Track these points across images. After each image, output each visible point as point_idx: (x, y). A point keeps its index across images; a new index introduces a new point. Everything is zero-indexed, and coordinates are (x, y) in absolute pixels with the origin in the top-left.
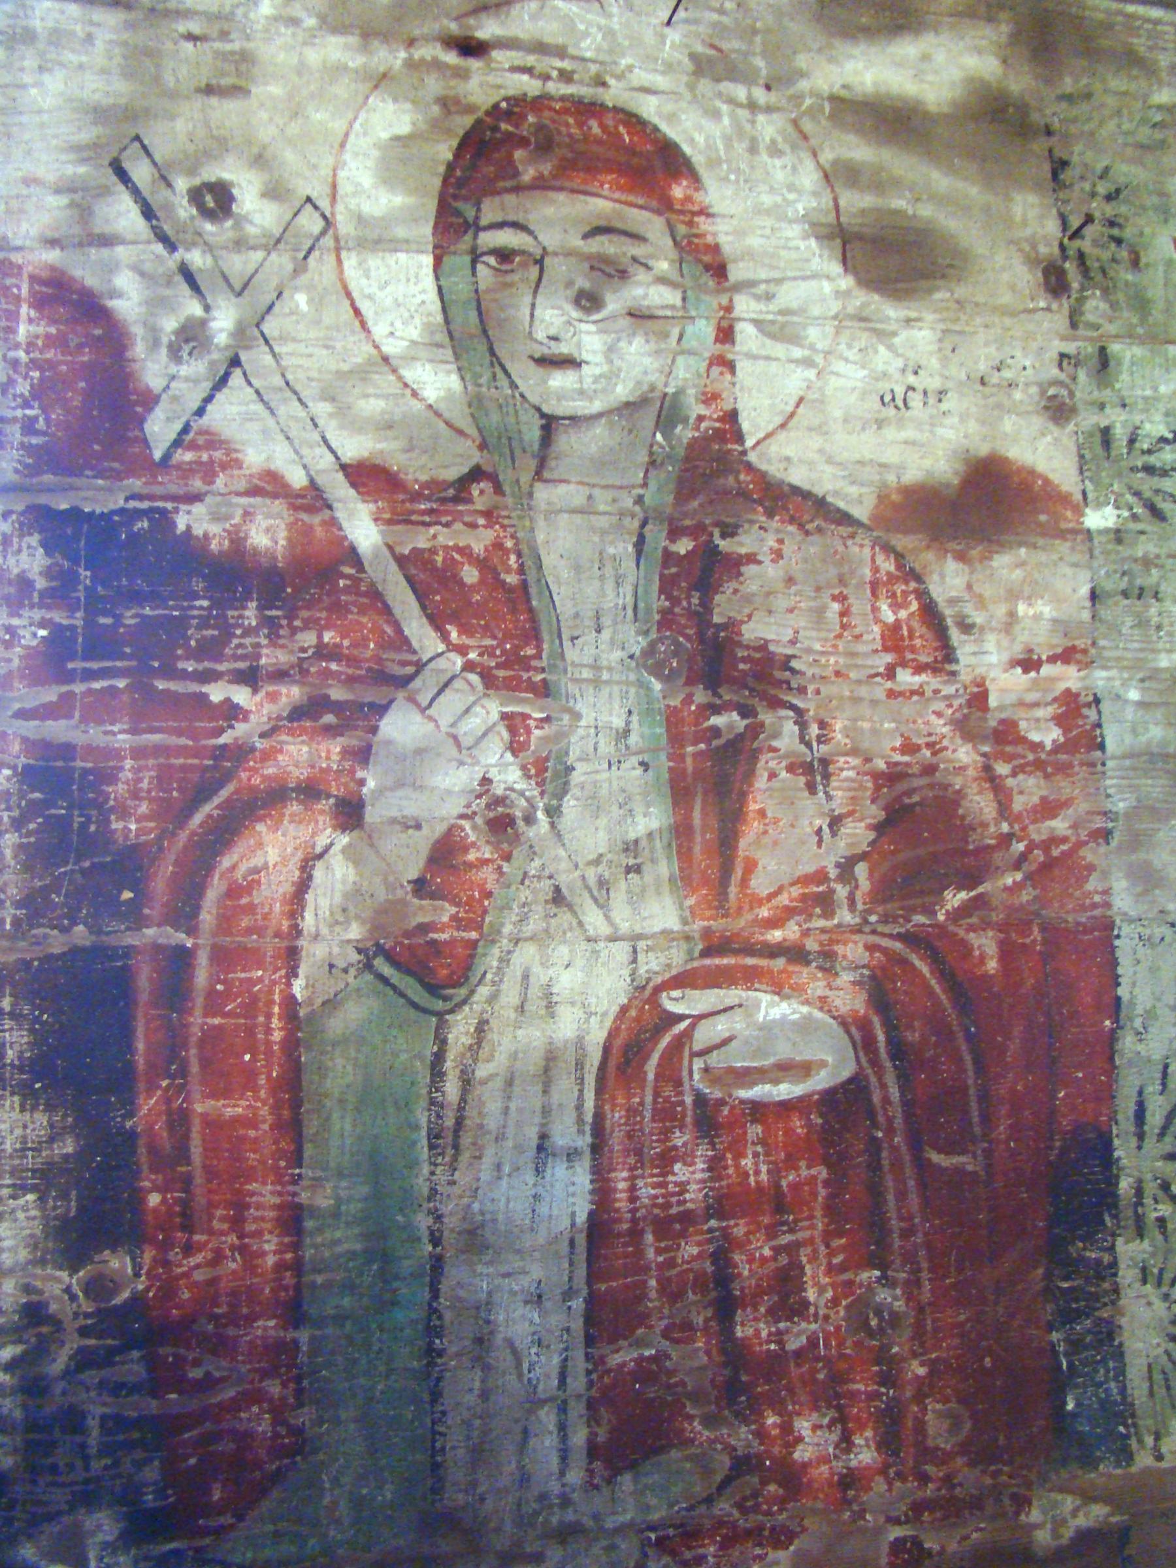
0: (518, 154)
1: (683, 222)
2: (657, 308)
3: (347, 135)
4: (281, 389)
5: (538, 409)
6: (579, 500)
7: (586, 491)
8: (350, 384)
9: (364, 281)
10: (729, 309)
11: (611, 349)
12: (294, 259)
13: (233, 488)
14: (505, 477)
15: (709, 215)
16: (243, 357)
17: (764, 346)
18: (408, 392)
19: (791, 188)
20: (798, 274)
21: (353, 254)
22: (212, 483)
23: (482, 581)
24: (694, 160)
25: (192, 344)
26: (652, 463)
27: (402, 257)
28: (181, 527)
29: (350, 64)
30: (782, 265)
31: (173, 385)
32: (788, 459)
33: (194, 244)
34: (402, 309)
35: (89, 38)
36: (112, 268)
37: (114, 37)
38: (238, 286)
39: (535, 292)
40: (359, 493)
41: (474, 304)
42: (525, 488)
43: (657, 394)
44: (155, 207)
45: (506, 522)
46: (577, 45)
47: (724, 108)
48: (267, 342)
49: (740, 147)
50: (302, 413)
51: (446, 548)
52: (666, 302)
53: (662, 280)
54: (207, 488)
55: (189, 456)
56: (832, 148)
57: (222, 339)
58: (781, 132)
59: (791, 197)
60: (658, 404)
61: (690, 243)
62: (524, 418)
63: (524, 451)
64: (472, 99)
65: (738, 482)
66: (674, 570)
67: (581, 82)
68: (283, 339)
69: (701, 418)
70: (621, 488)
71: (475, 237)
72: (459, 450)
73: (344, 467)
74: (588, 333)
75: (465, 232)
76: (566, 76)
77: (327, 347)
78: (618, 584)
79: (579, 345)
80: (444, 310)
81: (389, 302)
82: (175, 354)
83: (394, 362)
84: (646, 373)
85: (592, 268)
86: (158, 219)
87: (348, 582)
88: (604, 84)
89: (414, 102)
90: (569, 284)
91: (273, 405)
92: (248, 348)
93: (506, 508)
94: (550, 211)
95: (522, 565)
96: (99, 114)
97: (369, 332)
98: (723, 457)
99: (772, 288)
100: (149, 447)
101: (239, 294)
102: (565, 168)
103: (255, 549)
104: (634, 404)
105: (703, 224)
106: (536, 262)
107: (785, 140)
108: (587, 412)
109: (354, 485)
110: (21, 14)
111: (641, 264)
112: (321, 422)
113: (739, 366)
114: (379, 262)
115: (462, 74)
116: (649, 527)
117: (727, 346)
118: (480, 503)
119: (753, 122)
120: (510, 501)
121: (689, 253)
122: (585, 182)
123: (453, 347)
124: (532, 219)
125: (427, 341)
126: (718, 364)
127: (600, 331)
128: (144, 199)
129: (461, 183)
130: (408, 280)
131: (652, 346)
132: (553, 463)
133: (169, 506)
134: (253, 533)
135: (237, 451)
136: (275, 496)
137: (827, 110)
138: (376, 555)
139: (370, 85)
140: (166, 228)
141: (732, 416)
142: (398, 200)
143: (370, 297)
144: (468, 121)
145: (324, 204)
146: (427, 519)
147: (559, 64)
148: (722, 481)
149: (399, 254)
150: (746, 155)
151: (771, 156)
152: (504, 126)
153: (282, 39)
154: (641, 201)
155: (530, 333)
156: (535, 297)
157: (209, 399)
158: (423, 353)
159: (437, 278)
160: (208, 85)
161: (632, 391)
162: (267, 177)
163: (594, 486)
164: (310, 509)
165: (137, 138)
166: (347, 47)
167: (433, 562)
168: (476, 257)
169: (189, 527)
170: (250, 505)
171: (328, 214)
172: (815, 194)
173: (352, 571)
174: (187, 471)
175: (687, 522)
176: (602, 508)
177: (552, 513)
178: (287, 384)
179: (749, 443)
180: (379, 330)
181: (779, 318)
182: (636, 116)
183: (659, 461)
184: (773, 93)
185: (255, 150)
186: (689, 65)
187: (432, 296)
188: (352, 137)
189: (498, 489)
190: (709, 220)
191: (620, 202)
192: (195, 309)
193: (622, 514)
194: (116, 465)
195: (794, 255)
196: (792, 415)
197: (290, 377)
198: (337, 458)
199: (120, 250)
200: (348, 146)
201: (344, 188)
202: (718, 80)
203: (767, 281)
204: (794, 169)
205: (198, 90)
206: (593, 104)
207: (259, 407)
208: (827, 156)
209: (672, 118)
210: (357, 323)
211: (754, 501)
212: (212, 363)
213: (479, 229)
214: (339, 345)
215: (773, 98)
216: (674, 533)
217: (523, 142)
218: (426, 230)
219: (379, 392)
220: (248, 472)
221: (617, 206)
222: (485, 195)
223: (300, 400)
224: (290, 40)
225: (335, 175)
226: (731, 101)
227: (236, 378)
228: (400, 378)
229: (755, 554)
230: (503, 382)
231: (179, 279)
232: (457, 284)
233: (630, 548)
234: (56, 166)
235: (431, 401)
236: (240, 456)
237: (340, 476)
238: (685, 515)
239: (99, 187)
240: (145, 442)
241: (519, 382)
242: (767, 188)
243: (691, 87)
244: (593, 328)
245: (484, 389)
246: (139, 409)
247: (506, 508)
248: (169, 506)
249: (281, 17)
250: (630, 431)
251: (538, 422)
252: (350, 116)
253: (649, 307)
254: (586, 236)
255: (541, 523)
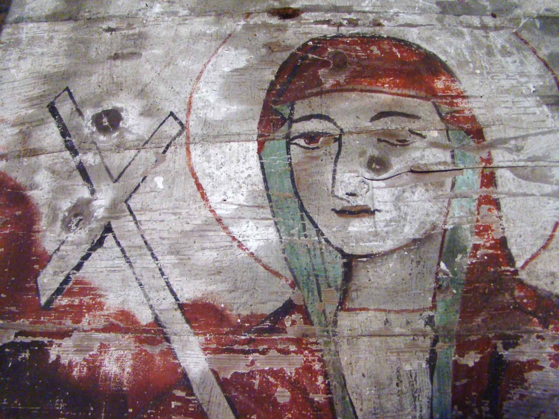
0: (321, 72)
1: (446, 103)
2: (432, 164)
3: (201, 72)
4: (140, 247)
5: (341, 251)
6: (376, 325)
7: (382, 316)
8: (192, 240)
9: (206, 165)
10: (489, 160)
11: (398, 199)
12: (157, 153)
13: (94, 326)
14: (313, 308)
15: (464, 97)
16: (114, 225)
17: (520, 186)
18: (235, 244)
19: (522, 74)
20: (538, 131)
21: (198, 146)
22: (79, 322)
23: (293, 400)
24: (448, 63)
25: (79, 218)
26: (439, 288)
27: (235, 145)
28: (53, 357)
29: (208, 32)
30: (524, 125)
31: (62, 248)
32: (553, 274)
33: (90, 149)
34: (233, 182)
35: (51, 39)
36: (35, 171)
37: (65, 36)
38: (115, 175)
39: (336, 162)
40: (192, 327)
41: (289, 173)
42: (330, 317)
43: (439, 230)
44: (69, 129)
45: (314, 347)
46: (359, 5)
47: (465, 30)
48: (131, 213)
49: (481, 53)
50: (153, 265)
51: (262, 372)
52: (439, 160)
53: (435, 144)
54: (75, 326)
55: (65, 301)
56: (547, 47)
57: (100, 213)
58: (509, 40)
59: (523, 80)
60: (440, 239)
61: (453, 117)
62: (328, 259)
63: (329, 286)
64: (288, 42)
65: (514, 298)
66: (464, 381)
67: (364, 25)
68: (142, 209)
69: (476, 247)
70: (413, 311)
71: (290, 127)
72: (275, 289)
73: (181, 306)
74: (379, 188)
75: (282, 125)
76: (353, 23)
77: (175, 214)
78: (415, 398)
79: (372, 198)
80: (265, 180)
81: (223, 178)
82: (67, 227)
83: (225, 222)
84: (428, 215)
85: (379, 140)
86: (70, 136)
87: (179, 404)
88: (379, 25)
89: (248, 48)
90: (362, 154)
91: (131, 260)
92: (117, 218)
93: (314, 335)
94: (345, 105)
95: (328, 385)
96: (47, 78)
97: (207, 200)
98: (498, 278)
99: (520, 143)
100: (39, 296)
101: (116, 181)
102: (354, 77)
103: (106, 375)
104: (419, 240)
105: (462, 104)
106: (336, 140)
107: (511, 46)
108: (381, 250)
109: (188, 321)
110: (16, 33)
111: (417, 134)
112: (166, 271)
113: (502, 203)
114: (217, 150)
115: (281, 29)
116: (440, 344)
117: (491, 189)
118: (292, 332)
119: (487, 37)
120: (317, 328)
121: (452, 124)
122: (370, 84)
123: (271, 207)
124: (332, 112)
125: (251, 204)
126: (486, 204)
127: (388, 186)
128: (64, 124)
129: (280, 94)
130: (238, 161)
131: (432, 193)
132: (354, 295)
133: (46, 340)
134: (106, 362)
135: (100, 296)
136: (126, 331)
137: (538, 25)
138: (203, 380)
139: (220, 42)
140: (74, 140)
141: (502, 243)
142: (234, 108)
143: (210, 176)
144: (286, 55)
145: (182, 116)
146: (246, 348)
147: (348, 16)
148: (499, 299)
149: (232, 143)
150: (486, 57)
151: (503, 56)
152: (310, 56)
153: (165, 23)
154: (412, 93)
155: (333, 191)
156: (335, 165)
157: (86, 257)
158: (248, 213)
159: (260, 158)
160: (115, 54)
161: (417, 231)
162: (145, 102)
163: (389, 311)
164: (152, 342)
165: (67, 89)
166: (206, 23)
167: (251, 385)
168: (289, 140)
169: (58, 357)
170: (106, 339)
171: (184, 122)
172: (540, 76)
173: (183, 394)
174: (62, 312)
175: (473, 338)
176: (397, 330)
177: (354, 338)
178: (146, 242)
179: (519, 264)
180: (215, 199)
181: (529, 164)
182: (403, 41)
183: (445, 284)
184: (498, 19)
185: (140, 88)
186: (438, 9)
187: (257, 170)
188: (205, 74)
189: (308, 320)
190: (465, 101)
191: (398, 95)
192: (84, 193)
193: (415, 334)
194: (13, 309)
195: (532, 118)
196: (551, 237)
197: (147, 238)
198: (177, 299)
199: (42, 157)
200: (202, 79)
201: (197, 104)
202: (459, 15)
203: (516, 138)
204: (522, 63)
205: (110, 58)
206: (373, 37)
207: (122, 262)
208: (544, 52)
209: (429, 40)
210: (199, 195)
211: (530, 313)
212: (91, 230)
213: (292, 122)
214: (184, 212)
215: (498, 21)
216: (462, 350)
217: (325, 64)
218: (255, 125)
219: (213, 245)
220: (106, 313)
221: (395, 97)
222: (298, 98)
223: (152, 254)
224: (170, 24)
225: (191, 97)
226: (469, 26)
227: (109, 241)
228: (229, 233)
229: (536, 361)
230: (311, 231)
231: (77, 173)
232: (275, 161)
233: (424, 365)
234: (16, 111)
235: (252, 250)
236: (102, 300)
237: (178, 314)
238: (470, 331)
239: (38, 120)
240: (37, 290)
241: (324, 230)
242: (505, 77)
243: (440, 21)
244: (382, 184)
245: (296, 238)
246: (36, 267)
247: (314, 335)
248: (46, 340)
249: (166, 12)
250: (418, 263)
251: (341, 261)
252: (205, 61)
253: (426, 165)
254: (373, 119)
255: (344, 347)
